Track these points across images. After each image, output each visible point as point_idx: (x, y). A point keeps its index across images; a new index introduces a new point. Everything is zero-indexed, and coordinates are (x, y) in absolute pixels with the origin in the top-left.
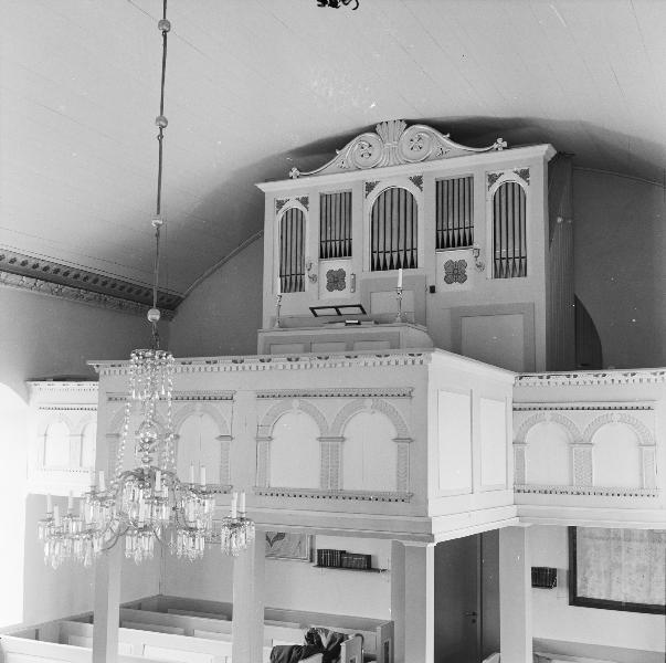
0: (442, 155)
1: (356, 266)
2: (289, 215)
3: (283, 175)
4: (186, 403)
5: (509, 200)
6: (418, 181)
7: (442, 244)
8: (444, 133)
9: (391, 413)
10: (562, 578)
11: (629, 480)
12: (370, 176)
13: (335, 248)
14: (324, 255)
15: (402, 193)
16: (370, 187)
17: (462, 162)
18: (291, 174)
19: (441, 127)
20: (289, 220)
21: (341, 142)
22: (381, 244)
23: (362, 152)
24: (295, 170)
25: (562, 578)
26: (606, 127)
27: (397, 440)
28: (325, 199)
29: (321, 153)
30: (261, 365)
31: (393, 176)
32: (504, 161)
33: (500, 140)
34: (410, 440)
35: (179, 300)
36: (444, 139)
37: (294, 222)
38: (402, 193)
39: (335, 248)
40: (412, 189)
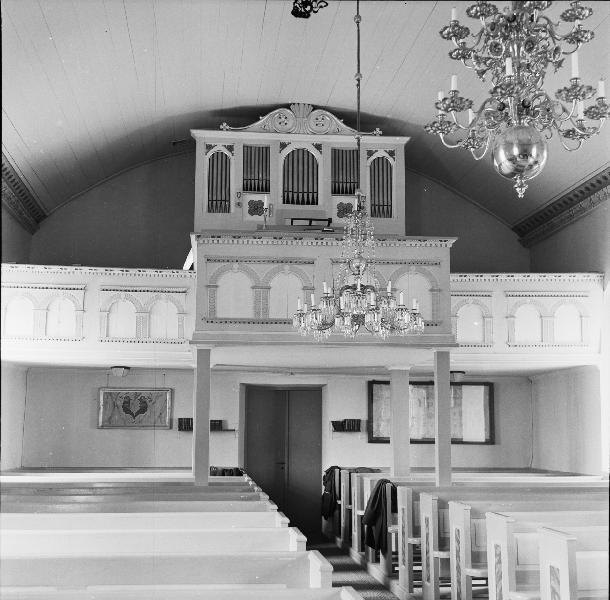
0: (337, 132)
1: (270, 199)
2: (291, 158)
3: (215, 127)
4: (276, 265)
5: (381, 168)
6: (318, 147)
7: (336, 191)
8: (340, 118)
9: (428, 275)
10: (363, 426)
11: (477, 338)
12: (284, 138)
13: (257, 184)
14: (247, 188)
15: (306, 154)
16: (283, 146)
17: (347, 139)
18: (221, 127)
19: (340, 114)
20: (215, 160)
21: (264, 111)
22: (290, 187)
23: (280, 120)
24: (225, 124)
25: (363, 426)
26: (169, 115)
27: (432, 290)
28: (247, 149)
29: (243, 117)
30: (335, 243)
31: (301, 141)
32: (377, 143)
33: (378, 129)
34: (440, 290)
35: (45, 216)
36: (340, 123)
37: (220, 163)
38: (306, 154)
39: (257, 184)
40: (314, 152)
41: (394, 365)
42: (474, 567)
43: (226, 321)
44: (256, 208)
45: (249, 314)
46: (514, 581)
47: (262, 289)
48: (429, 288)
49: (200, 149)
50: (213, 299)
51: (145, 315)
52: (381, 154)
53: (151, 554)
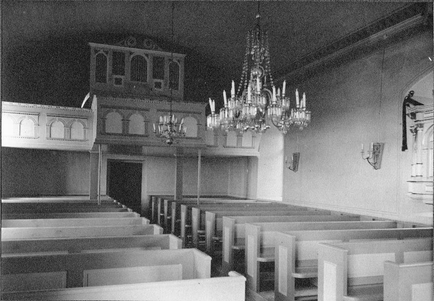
1: (126, 78)
5: (174, 68)
6: (147, 55)
28: (115, 53)
37: (101, 60)
41: (370, 147)
42: (261, 257)
43: (108, 134)
44: (118, 81)
45: (120, 132)
46: (259, 270)
47: (126, 122)
48: (122, 119)
49: (92, 52)
50: (104, 126)
51: (69, 128)
52: (101, 52)
53: (315, 207)
